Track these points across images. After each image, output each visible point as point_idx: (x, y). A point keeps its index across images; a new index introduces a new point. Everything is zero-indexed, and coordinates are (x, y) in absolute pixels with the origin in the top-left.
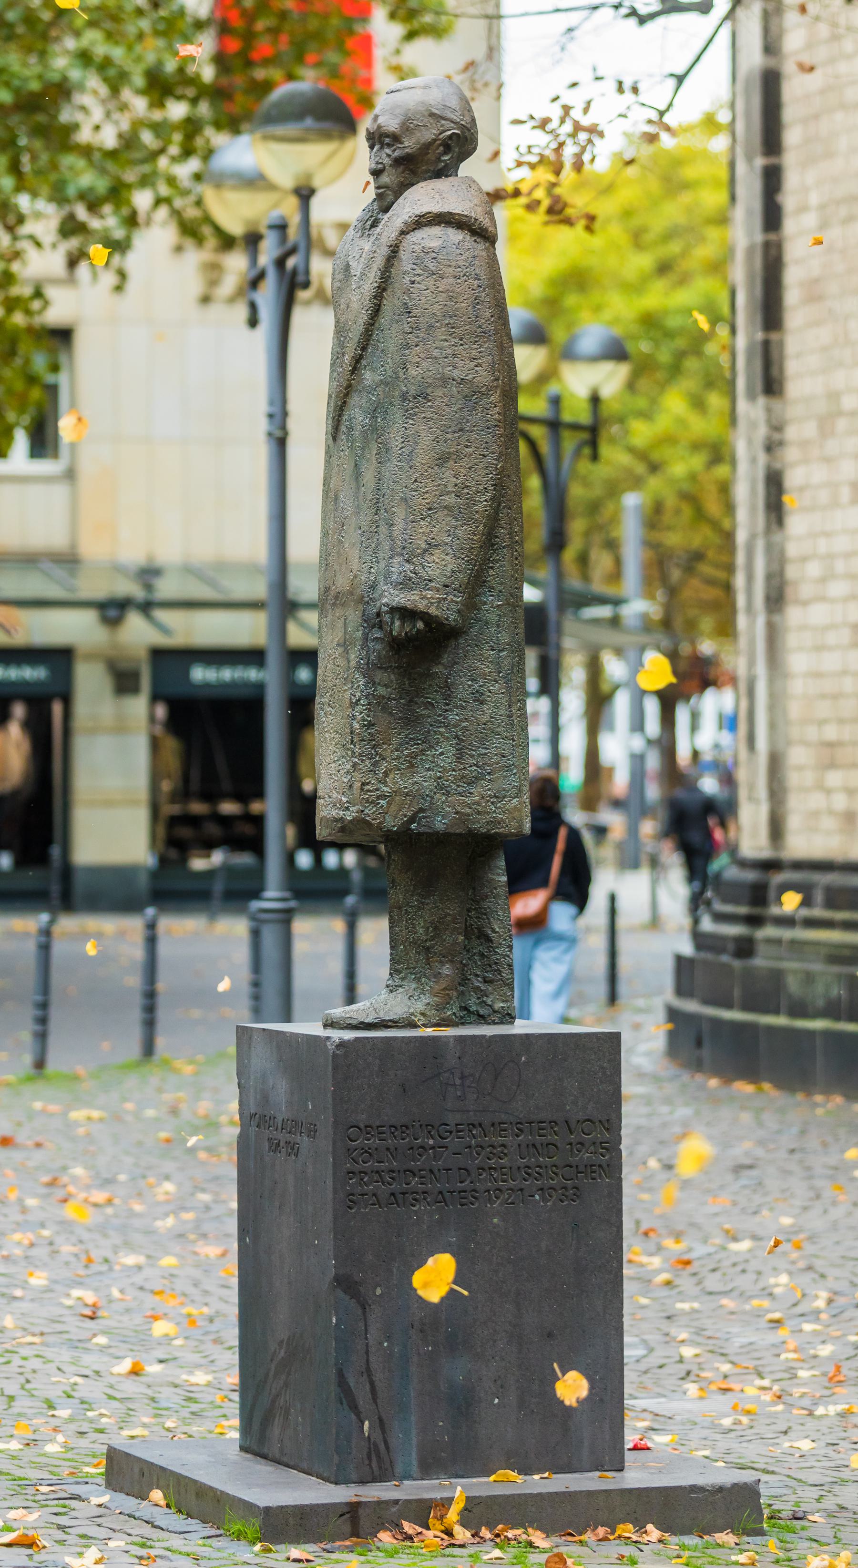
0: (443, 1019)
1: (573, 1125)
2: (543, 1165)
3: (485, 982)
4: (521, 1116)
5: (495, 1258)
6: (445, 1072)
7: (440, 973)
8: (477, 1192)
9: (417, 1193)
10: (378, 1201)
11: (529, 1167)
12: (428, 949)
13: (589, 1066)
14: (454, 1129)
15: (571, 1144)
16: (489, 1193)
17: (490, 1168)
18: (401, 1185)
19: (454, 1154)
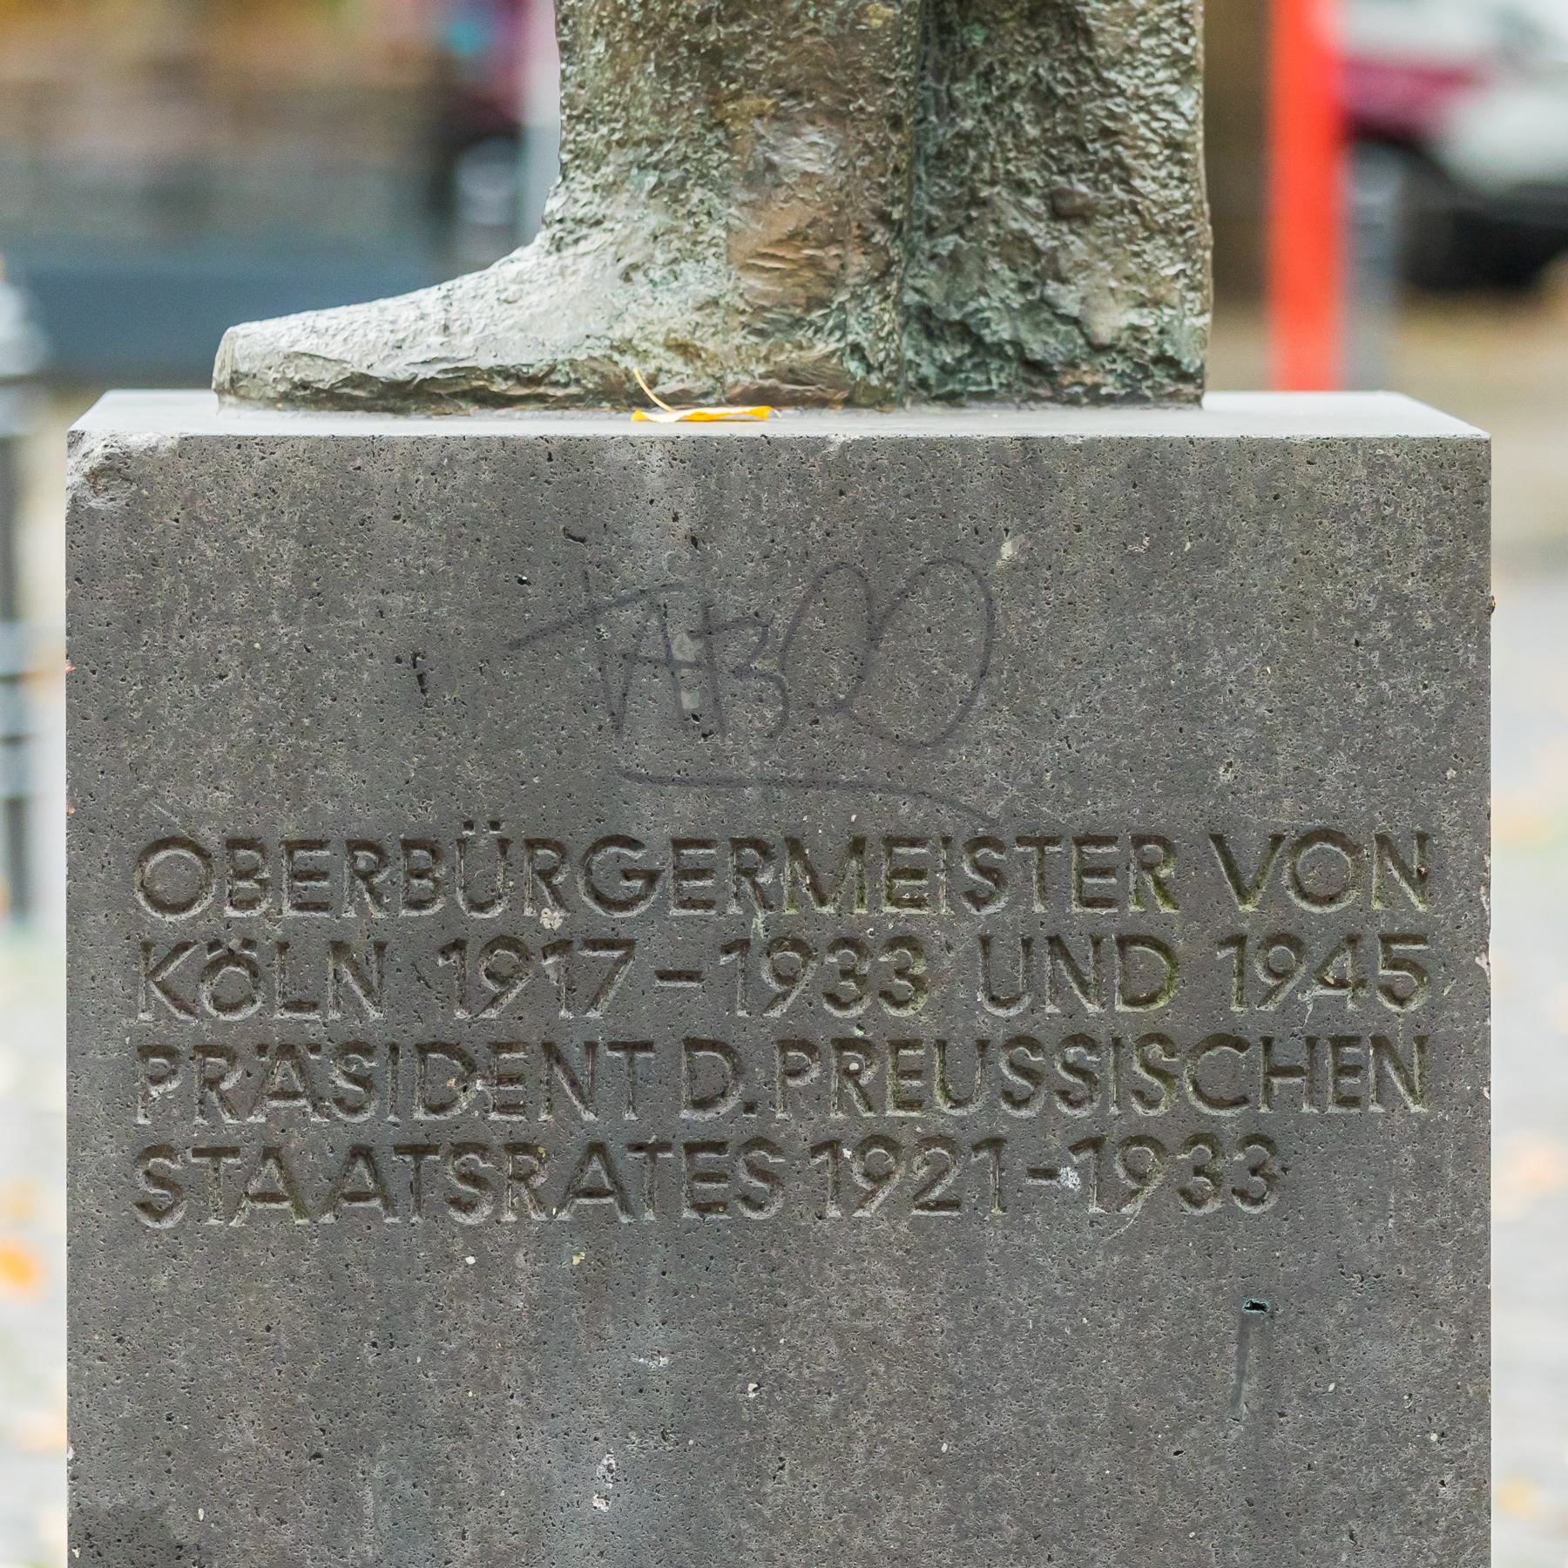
0: (792, 375)
1: (1250, 852)
2: (1102, 1035)
3: (1057, 214)
4: (994, 811)
5: (859, 1449)
6: (622, 603)
7: (771, 166)
8: (775, 1150)
9: (482, 1149)
10: (289, 1182)
11: (1033, 1044)
12: (715, 57)
13: (1329, 592)
14: (663, 861)
15: (1239, 941)
16: (836, 1155)
17: (843, 1044)
18: (404, 1111)
19: (664, 975)
